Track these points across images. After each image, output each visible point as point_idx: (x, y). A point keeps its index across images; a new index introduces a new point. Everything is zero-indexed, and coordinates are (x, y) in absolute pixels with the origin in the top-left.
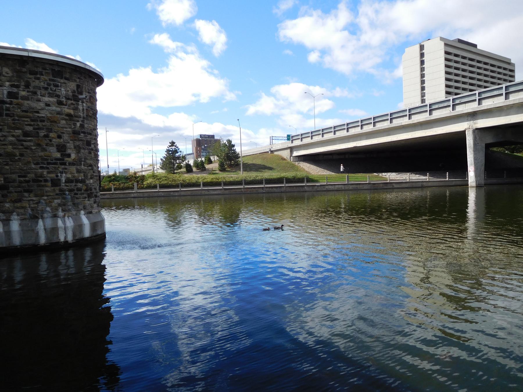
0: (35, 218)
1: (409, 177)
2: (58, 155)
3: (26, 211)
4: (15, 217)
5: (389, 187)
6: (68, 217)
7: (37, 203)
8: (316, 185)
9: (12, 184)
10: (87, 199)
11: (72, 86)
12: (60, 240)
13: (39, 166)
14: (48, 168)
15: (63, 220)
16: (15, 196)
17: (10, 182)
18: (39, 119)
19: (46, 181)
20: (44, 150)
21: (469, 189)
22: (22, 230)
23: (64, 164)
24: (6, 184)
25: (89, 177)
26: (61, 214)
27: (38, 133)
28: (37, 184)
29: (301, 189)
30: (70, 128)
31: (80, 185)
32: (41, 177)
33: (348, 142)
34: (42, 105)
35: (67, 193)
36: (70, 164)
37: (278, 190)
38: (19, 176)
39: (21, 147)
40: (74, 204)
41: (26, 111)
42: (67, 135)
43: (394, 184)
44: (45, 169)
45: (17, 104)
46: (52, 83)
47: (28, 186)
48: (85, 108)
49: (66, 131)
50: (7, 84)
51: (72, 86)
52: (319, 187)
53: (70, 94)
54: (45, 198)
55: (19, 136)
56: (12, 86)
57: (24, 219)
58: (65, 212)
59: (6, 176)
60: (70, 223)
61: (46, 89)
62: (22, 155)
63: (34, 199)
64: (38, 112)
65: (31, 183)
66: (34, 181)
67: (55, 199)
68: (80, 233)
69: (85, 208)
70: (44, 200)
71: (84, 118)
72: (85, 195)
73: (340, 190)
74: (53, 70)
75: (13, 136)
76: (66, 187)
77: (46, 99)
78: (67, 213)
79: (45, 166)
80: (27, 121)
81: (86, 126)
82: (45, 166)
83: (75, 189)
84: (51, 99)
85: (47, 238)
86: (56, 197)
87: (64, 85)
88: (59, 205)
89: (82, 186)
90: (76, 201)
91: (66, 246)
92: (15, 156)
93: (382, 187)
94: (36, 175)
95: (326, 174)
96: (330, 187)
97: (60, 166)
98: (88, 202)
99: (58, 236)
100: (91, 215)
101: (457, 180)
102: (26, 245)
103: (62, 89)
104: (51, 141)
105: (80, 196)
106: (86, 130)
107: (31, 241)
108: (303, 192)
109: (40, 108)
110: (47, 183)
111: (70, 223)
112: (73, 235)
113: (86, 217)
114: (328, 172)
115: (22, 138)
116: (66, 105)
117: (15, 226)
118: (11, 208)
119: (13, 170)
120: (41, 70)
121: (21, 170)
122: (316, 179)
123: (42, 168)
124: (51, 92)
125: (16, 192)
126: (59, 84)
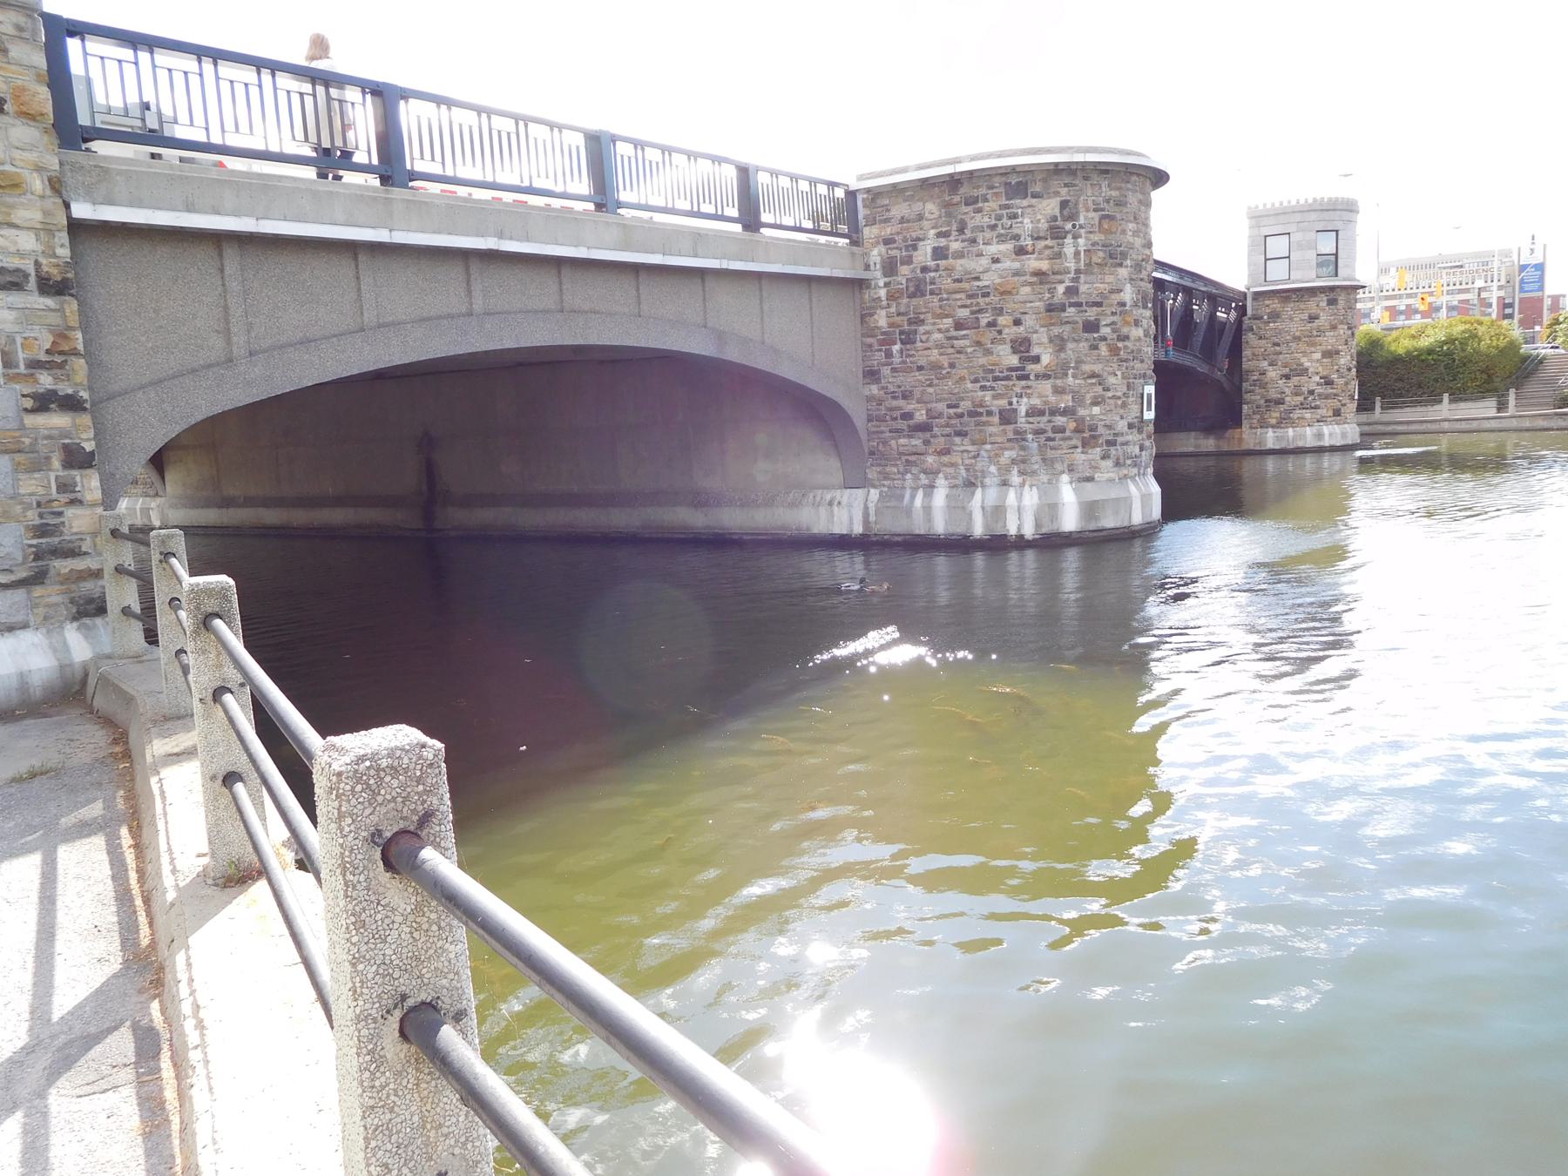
0: (970, 485)
2: (1014, 360)
4: (941, 481)
6: (1031, 486)
7: (974, 457)
10: (1079, 450)
11: (1050, 206)
13: (979, 385)
14: (993, 388)
15: (1019, 491)
16: (940, 442)
18: (980, 292)
19: (990, 413)
20: (988, 352)
23: (1026, 377)
25: (1088, 402)
26: (1015, 479)
27: (977, 319)
30: (1040, 300)
31: (1060, 420)
32: (982, 406)
34: (985, 262)
35: (1030, 437)
36: (1037, 377)
38: (949, 406)
39: (951, 350)
40: (1044, 460)
41: (959, 281)
42: (1034, 317)
45: (947, 269)
46: (1004, 212)
48: (1082, 249)
49: (1031, 308)
50: (932, 232)
51: (1050, 206)
53: (1044, 225)
55: (948, 330)
56: (939, 235)
57: (955, 486)
59: (929, 406)
60: (1031, 498)
61: (993, 227)
62: (952, 366)
63: (970, 448)
64: (977, 279)
65: (966, 419)
66: (972, 414)
67: (1006, 449)
68: (1052, 521)
69: (1071, 470)
70: (986, 451)
71: (1078, 271)
72: (1074, 442)
74: (1007, 184)
75: (940, 330)
76: (1027, 425)
77: (994, 249)
79: (988, 384)
80: (961, 299)
81: (1083, 288)
82: (988, 384)
83: (1049, 429)
84: (1002, 247)
85: (986, 526)
86: (1008, 445)
87: (1029, 210)
88: (1014, 462)
89: (1068, 422)
90: (1050, 454)
91: (1021, 543)
92: (941, 367)
97: (1017, 382)
98: (1083, 457)
102: (953, 535)
103: (1025, 221)
104: (1000, 332)
105: (1061, 443)
106: (1082, 299)
107: (959, 529)
109: (981, 270)
110: (989, 419)
111: (1031, 498)
113: (1074, 489)
115: (953, 333)
116: (1033, 253)
117: (940, 497)
118: (935, 465)
120: (984, 192)
123: (983, 388)
124: (1002, 231)
125: (943, 436)
126: (1020, 211)
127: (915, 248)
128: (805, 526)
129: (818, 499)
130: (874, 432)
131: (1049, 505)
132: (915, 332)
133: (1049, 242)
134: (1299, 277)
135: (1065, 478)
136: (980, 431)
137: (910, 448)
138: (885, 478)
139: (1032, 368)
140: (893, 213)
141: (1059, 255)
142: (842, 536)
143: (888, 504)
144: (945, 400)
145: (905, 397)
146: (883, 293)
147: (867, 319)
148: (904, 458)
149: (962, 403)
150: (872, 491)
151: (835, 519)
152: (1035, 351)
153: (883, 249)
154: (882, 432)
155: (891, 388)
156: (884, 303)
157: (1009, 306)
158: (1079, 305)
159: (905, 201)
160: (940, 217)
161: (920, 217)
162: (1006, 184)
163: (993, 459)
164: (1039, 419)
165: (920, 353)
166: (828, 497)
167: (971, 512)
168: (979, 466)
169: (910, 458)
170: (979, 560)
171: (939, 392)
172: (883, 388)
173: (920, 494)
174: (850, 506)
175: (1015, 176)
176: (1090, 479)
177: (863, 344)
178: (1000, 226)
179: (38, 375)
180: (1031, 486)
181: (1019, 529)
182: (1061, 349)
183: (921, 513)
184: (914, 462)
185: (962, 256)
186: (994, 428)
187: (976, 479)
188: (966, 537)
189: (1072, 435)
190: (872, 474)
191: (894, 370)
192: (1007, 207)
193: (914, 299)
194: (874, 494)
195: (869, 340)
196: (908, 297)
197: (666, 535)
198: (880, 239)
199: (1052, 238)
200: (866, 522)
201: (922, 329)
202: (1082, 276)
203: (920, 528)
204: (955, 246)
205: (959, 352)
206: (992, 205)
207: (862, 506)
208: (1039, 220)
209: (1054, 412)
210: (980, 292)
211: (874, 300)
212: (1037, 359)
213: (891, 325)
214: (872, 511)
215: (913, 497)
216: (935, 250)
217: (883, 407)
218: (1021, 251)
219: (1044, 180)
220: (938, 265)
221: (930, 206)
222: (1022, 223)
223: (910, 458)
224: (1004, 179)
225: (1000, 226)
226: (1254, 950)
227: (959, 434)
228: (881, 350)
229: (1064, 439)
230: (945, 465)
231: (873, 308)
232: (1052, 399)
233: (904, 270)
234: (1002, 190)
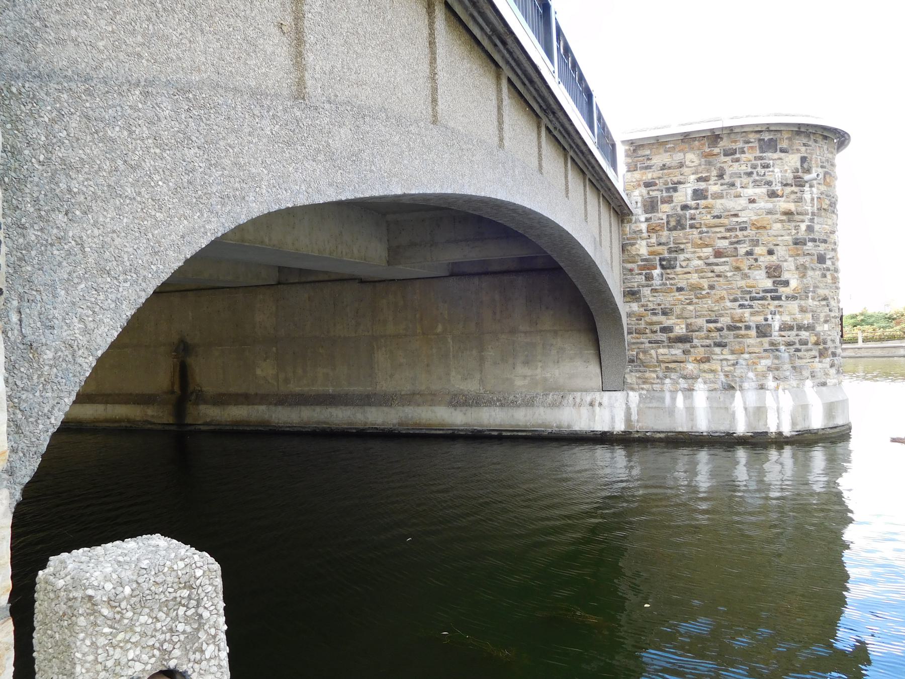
2: (768, 284)
3: (717, 376)
6: (784, 390)
7: (733, 365)
9: (697, 333)
10: (817, 360)
11: (793, 160)
12: (769, 428)
13: (738, 303)
14: (751, 307)
16: (700, 352)
19: (748, 328)
20: (746, 276)
22: (711, 407)
23: (779, 298)
25: (822, 320)
26: (771, 383)
27: (736, 248)
28: (734, 332)
30: (789, 234)
31: (804, 334)
32: (741, 321)
34: (743, 202)
35: (782, 348)
36: (787, 298)
38: (708, 322)
40: (794, 368)
45: (707, 207)
46: (759, 162)
47: (721, 336)
48: (815, 196)
51: (793, 160)
53: (790, 175)
55: (708, 258)
56: (699, 180)
58: (778, 382)
59: (689, 321)
60: (787, 401)
61: (750, 174)
62: (712, 287)
63: (730, 357)
64: (736, 215)
65: (725, 332)
66: (730, 328)
75: (700, 258)
77: (750, 192)
78: (782, 383)
79: (746, 303)
81: (817, 227)
83: (797, 341)
85: (749, 424)
86: (765, 354)
88: (769, 369)
90: (798, 363)
91: (780, 442)
92: (702, 289)
99: (766, 421)
100: (824, 388)
104: (756, 260)
105: (805, 353)
106: (816, 236)
107: (722, 427)
109: (740, 208)
110: (748, 332)
111: (787, 401)
112: (792, 422)
113: (816, 392)
115: (712, 260)
116: (782, 196)
117: (701, 397)
123: (741, 306)
124: (757, 178)
125: (702, 346)
126: (771, 162)
127: (675, 190)
129: (578, 400)
130: (634, 343)
131: (802, 406)
132: (676, 259)
133: (794, 189)
135: (809, 383)
136: (740, 343)
137: (669, 357)
138: (644, 383)
139: (783, 290)
140: (652, 162)
141: (800, 200)
143: (651, 405)
144: (704, 316)
145: (664, 313)
146: (644, 227)
147: (629, 248)
148: (663, 366)
149: (722, 319)
150: (631, 393)
152: (785, 276)
153: (644, 191)
154: (642, 343)
155: (651, 306)
156: (645, 235)
157: (764, 238)
158: (814, 240)
159: (666, 151)
160: (700, 165)
161: (681, 165)
162: (760, 140)
163: (752, 366)
164: (789, 333)
165: (680, 276)
166: (588, 398)
168: (738, 372)
169: (670, 365)
170: (742, 454)
171: (699, 309)
172: (643, 306)
173: (680, 397)
174: (611, 407)
175: (767, 134)
176: (824, 384)
177: (624, 268)
178: (755, 173)
180: (784, 390)
181: (778, 427)
182: (804, 276)
183: (684, 412)
185: (722, 197)
186: (752, 340)
187: (736, 383)
188: (730, 434)
189: (812, 346)
190: (631, 379)
191: (654, 291)
192: (761, 158)
193: (674, 232)
194: (634, 397)
195: (629, 266)
196: (670, 230)
197: (423, 432)
198: (642, 183)
199: (796, 185)
200: (628, 420)
201: (681, 257)
202: (815, 217)
203: (682, 425)
204: (714, 188)
205: (718, 276)
206: (749, 156)
207: (624, 406)
208: (786, 171)
209: (800, 328)
210: (738, 227)
211: (635, 232)
212: (786, 283)
213: (651, 253)
214: (634, 411)
215: (674, 399)
216: (695, 192)
217: (642, 322)
218: (773, 195)
219: (790, 139)
220: (698, 204)
221: (690, 156)
222: (773, 171)
223: (670, 365)
224: (758, 136)
225: (755, 173)
226: (548, 523)
227: (719, 345)
228: (641, 274)
229: (807, 350)
231: (634, 239)
232: (799, 316)
233: (666, 208)
234: (756, 144)
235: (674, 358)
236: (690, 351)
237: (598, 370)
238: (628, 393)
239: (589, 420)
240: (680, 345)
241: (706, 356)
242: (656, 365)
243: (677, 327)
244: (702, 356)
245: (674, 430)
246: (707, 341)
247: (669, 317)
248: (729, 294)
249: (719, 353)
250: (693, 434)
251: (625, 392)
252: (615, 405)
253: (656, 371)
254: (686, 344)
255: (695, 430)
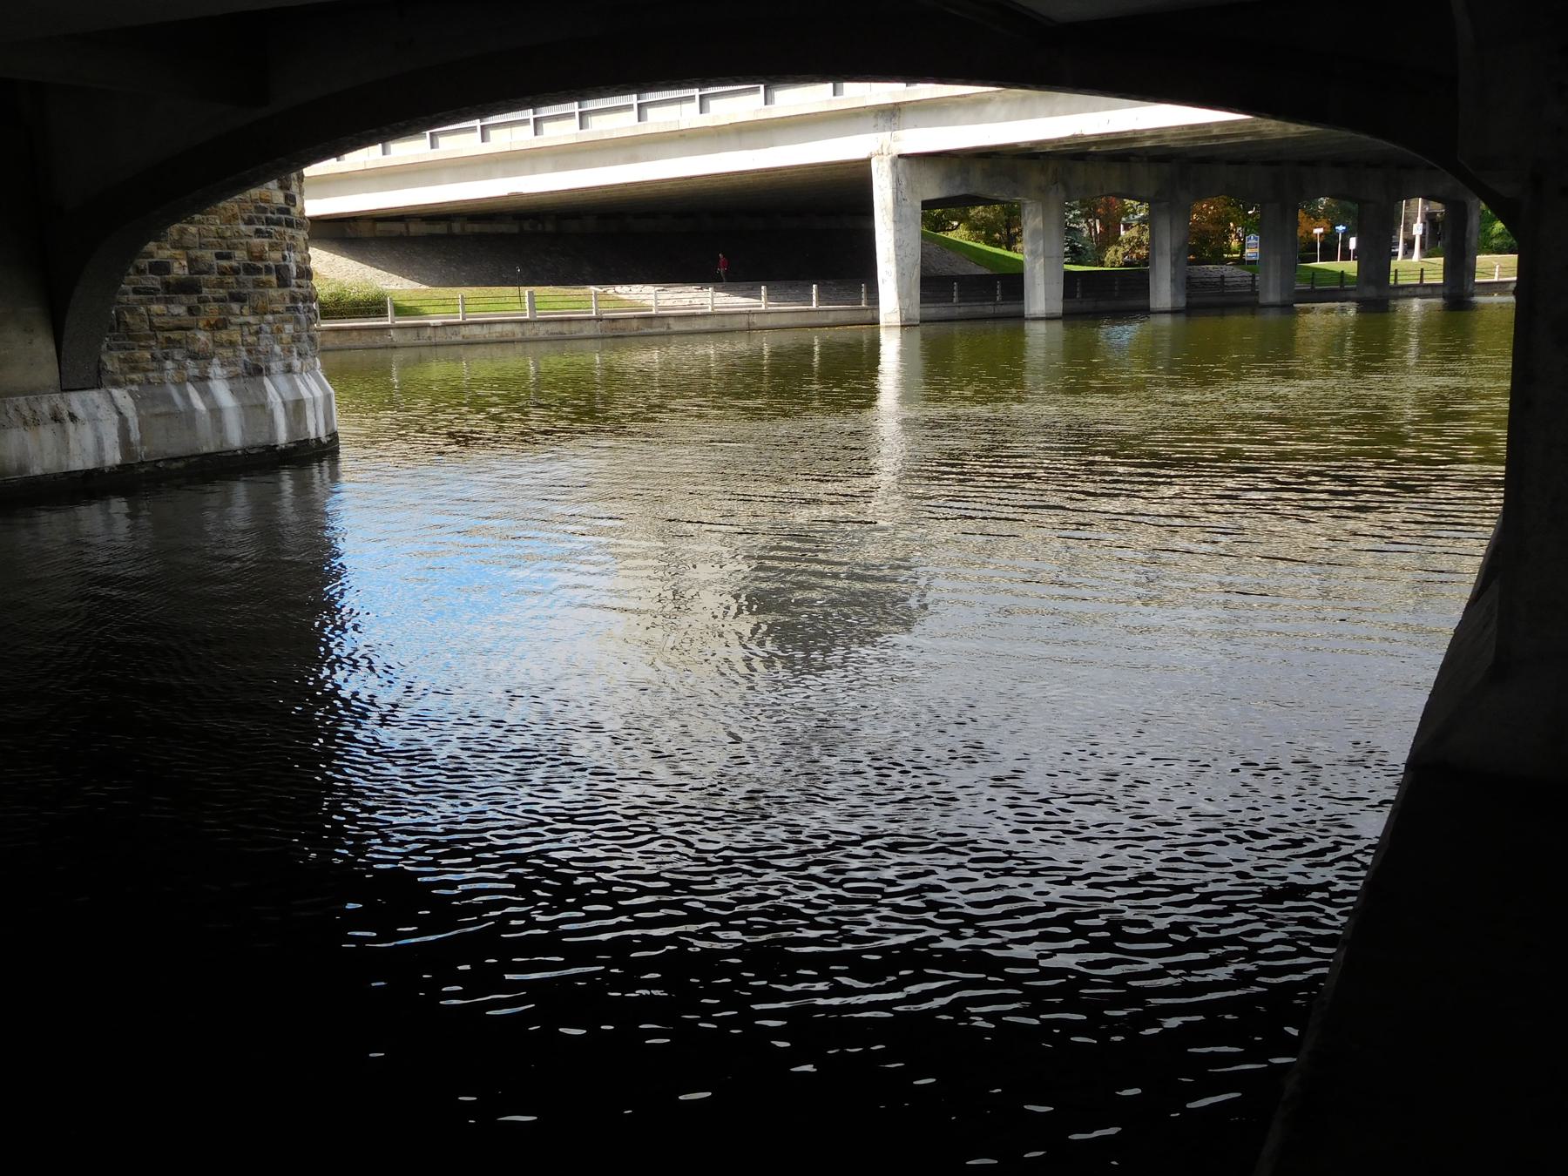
0: (257, 371)
1: (657, 299)
3: (237, 353)
5: (657, 330)
7: (257, 333)
8: (427, 326)
9: (206, 277)
17: (201, 272)
21: (882, 332)
22: (243, 406)
24: (195, 276)
28: (254, 277)
29: (379, 340)
33: (488, 176)
37: (367, 339)
38: (219, 256)
43: (671, 321)
44: (265, 237)
47: (238, 282)
52: (440, 332)
54: (270, 318)
57: (237, 376)
59: (193, 253)
63: (251, 319)
73: (507, 342)
93: (638, 329)
94: (250, 252)
95: (398, 288)
96: (476, 330)
101: (839, 310)
107: (262, 440)
108: (386, 347)
114: (406, 281)
119: (205, 237)
121: (220, 237)
122: (408, 304)
123: (259, 233)
125: (216, 300)
128: (15, 464)
134: (517, 130)
138: (134, 370)
142: (87, 474)
143: (157, 410)
148: (160, 335)
150: (116, 392)
151: (72, 445)
167: (272, 410)
179: (246, 258)
183: (208, 419)
184: (179, 342)
190: (112, 362)
214: (134, 423)
215: (186, 397)
223: (175, 335)
230: (222, 345)
235: (176, 322)
236: (199, 308)
237: (52, 350)
238: (110, 393)
239: (58, 451)
240: (183, 297)
241: (222, 317)
242: (149, 335)
243: (176, 265)
244: (217, 317)
245: (196, 452)
246: (221, 291)
247: (163, 245)
248: (242, 210)
249: (238, 312)
250: (224, 455)
251: (103, 390)
252: (99, 415)
253: (150, 347)
254: (192, 296)
255: (226, 447)
